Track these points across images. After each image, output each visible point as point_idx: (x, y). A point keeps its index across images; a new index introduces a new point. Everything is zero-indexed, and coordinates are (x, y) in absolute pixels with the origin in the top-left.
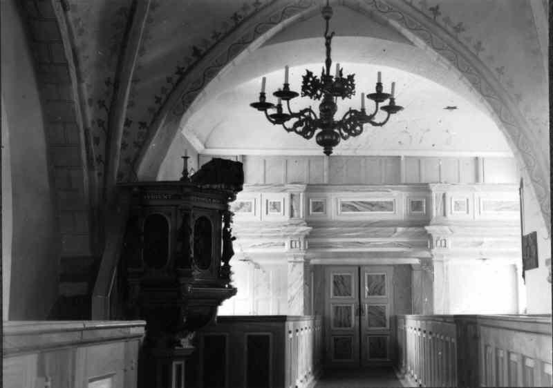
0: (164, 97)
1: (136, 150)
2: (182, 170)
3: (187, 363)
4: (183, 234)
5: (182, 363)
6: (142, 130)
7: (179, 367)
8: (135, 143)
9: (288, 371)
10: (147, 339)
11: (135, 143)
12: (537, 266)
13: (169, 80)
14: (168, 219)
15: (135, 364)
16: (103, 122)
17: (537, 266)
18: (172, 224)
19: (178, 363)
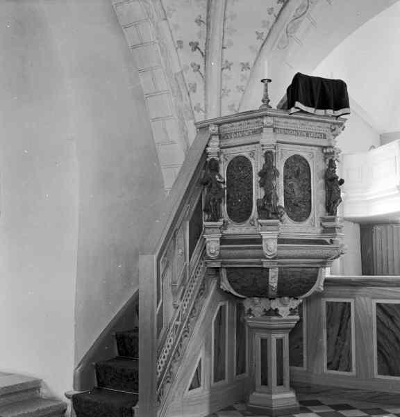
0: (266, 32)
1: (240, 94)
2: (261, 97)
3: (291, 335)
4: (267, 174)
5: (285, 336)
6: (244, 72)
7: (280, 342)
8: (237, 87)
9: (269, 366)
10: (319, 293)
11: (237, 87)
12: (298, 77)
13: (270, 11)
14: (252, 160)
15: (77, 382)
16: (199, 67)
17: (298, 77)
18: (257, 165)
19: (280, 336)
